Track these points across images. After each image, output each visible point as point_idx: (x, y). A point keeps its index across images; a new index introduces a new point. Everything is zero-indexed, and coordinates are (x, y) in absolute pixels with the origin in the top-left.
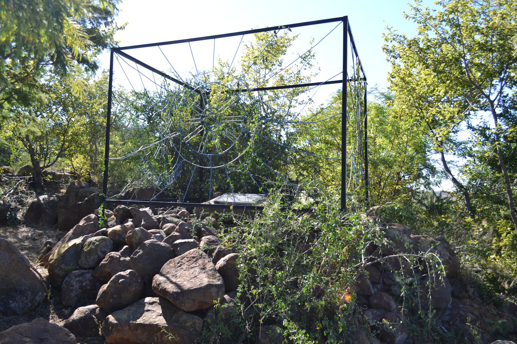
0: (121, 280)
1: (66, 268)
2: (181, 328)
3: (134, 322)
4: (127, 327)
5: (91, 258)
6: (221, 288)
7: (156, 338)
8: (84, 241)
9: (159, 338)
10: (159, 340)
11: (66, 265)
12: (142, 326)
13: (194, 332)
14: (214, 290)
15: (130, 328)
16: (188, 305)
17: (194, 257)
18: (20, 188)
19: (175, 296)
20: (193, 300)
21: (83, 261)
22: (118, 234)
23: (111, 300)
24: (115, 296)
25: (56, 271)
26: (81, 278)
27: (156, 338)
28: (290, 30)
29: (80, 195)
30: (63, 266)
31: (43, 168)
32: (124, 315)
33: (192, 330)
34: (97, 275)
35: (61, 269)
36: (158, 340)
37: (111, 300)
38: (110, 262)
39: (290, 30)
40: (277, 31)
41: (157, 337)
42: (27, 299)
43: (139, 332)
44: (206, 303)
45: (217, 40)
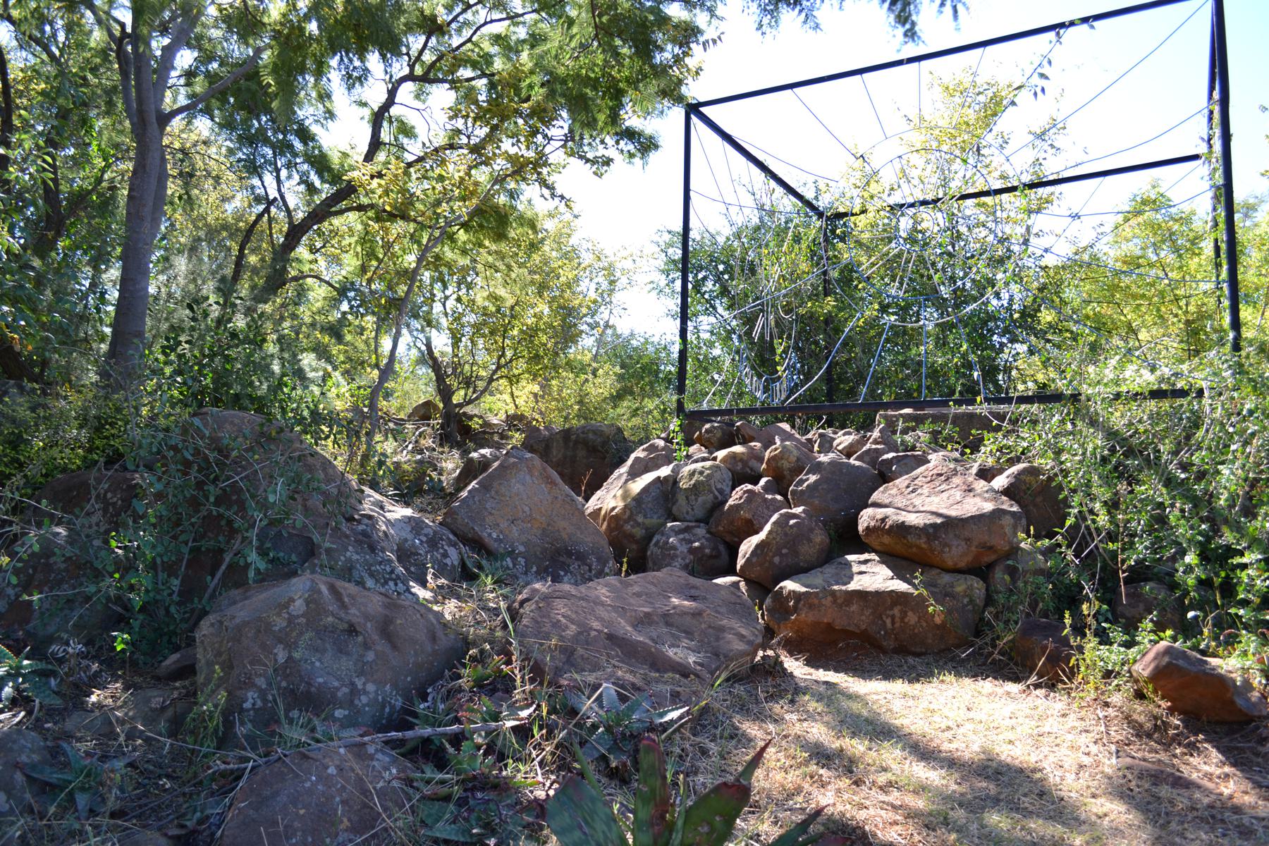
0: (792, 522)
1: (648, 521)
2: (946, 595)
3: (844, 588)
4: (829, 598)
5: (700, 499)
6: (1020, 519)
7: (888, 621)
8: (676, 471)
9: (897, 619)
10: (897, 625)
11: (645, 517)
12: (862, 595)
13: (970, 607)
14: (1008, 521)
15: (835, 602)
16: (956, 553)
17: (941, 475)
18: (423, 442)
19: (931, 530)
20: (968, 540)
21: (681, 504)
22: (741, 460)
23: (777, 560)
24: (784, 551)
25: (628, 527)
26: (686, 536)
27: (888, 621)
28: (1092, 27)
29: (573, 437)
30: (640, 519)
31: (460, 405)
32: (818, 578)
33: (966, 600)
34: (721, 528)
35: (638, 524)
36: (893, 623)
37: (777, 560)
38: (749, 500)
39: (1092, 27)
40: (1062, 31)
41: (893, 617)
42: (590, 571)
43: (854, 608)
44: (991, 548)
45: (692, 187)
